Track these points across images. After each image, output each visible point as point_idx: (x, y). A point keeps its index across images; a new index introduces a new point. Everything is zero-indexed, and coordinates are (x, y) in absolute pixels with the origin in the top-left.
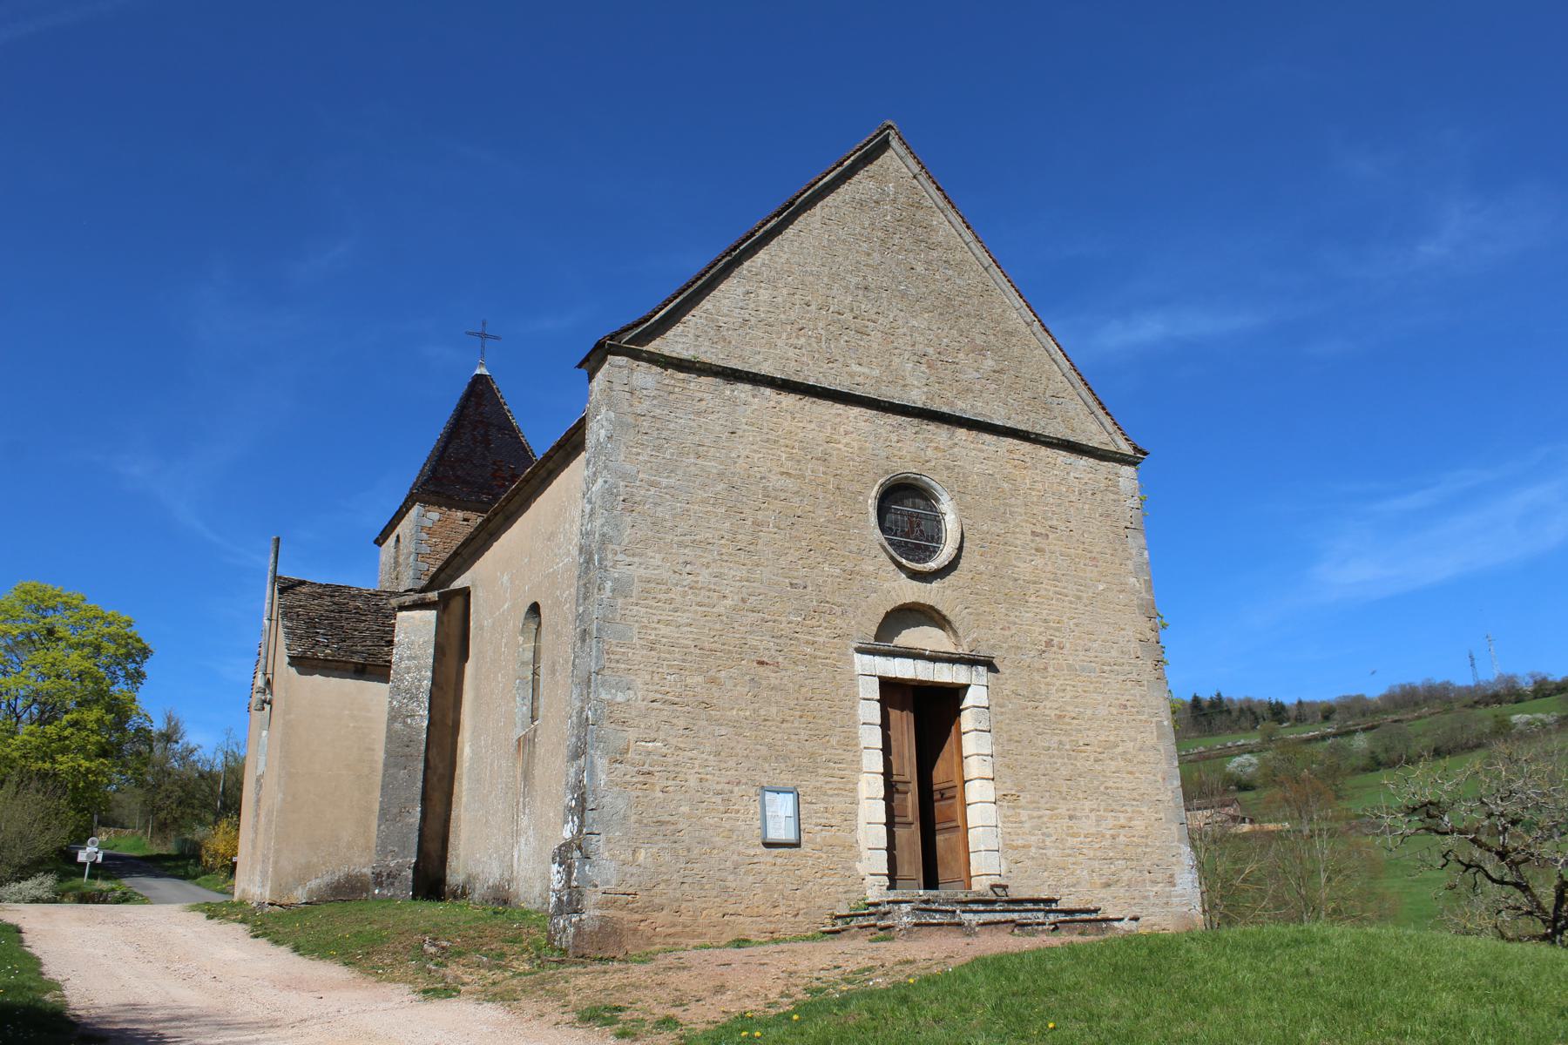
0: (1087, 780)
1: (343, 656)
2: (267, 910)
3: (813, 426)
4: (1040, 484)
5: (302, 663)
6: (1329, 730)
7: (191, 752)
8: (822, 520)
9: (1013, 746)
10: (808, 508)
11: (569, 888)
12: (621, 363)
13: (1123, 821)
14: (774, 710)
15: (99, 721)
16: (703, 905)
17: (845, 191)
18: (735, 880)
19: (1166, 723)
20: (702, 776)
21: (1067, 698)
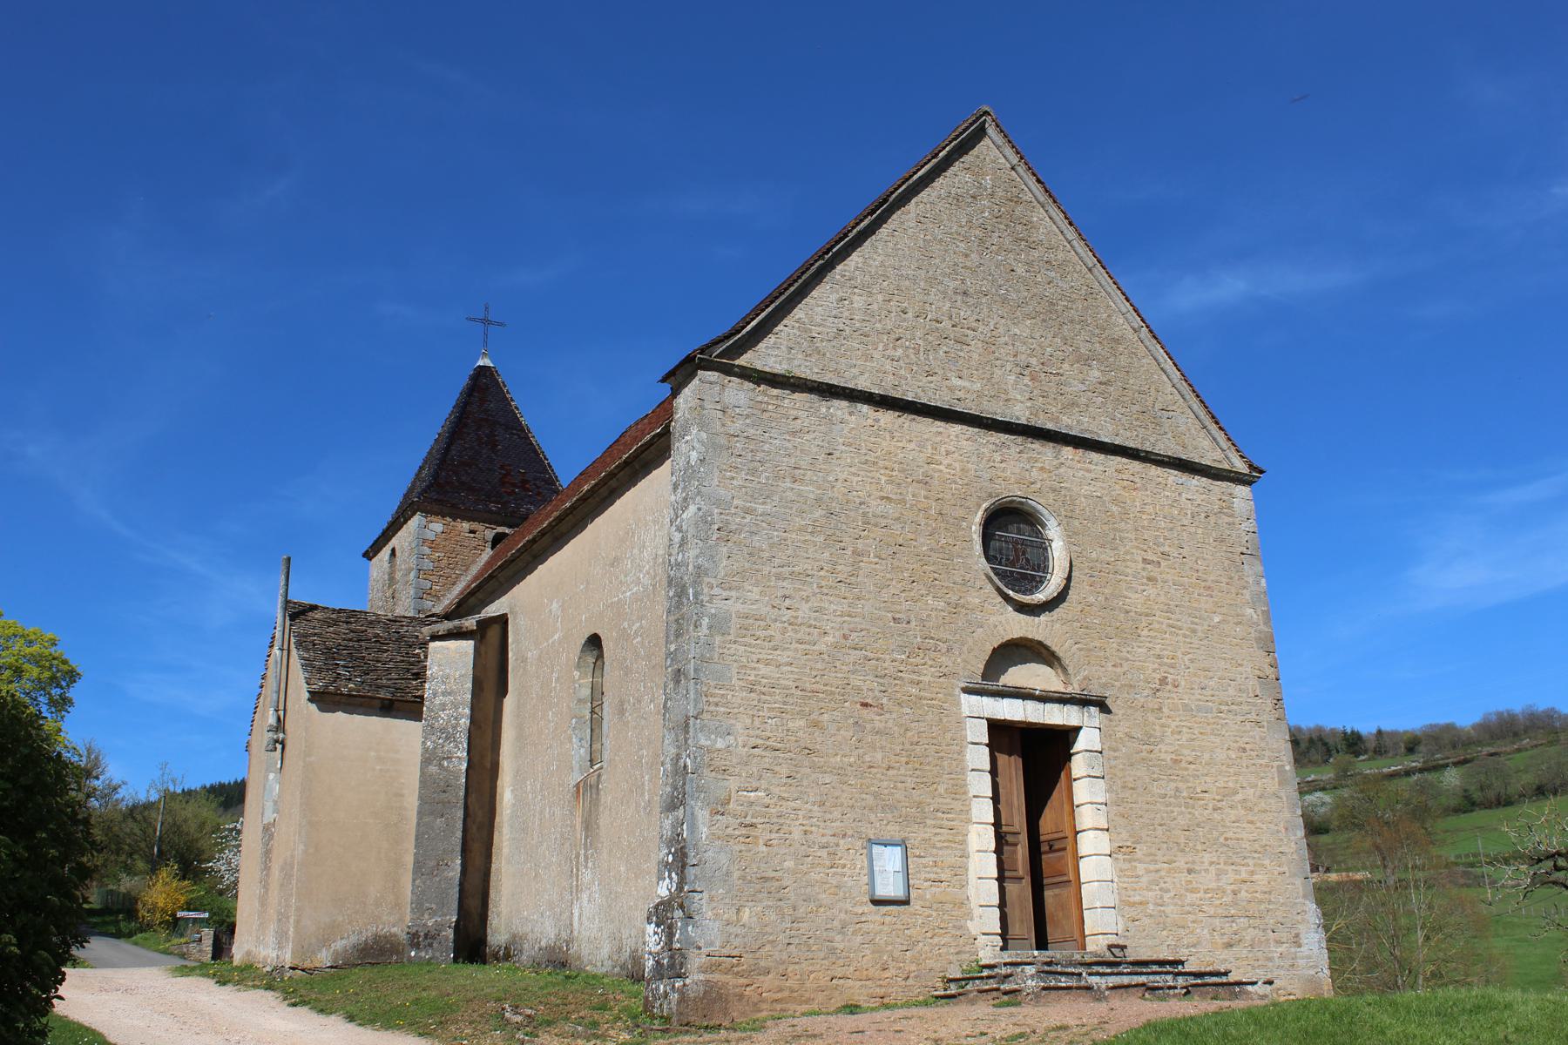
0: (1205, 830)
1: (369, 691)
2: (288, 975)
3: (912, 446)
4: (1151, 507)
5: (325, 699)
6: (1414, 764)
7: (115, 789)
8: (924, 549)
9: (1127, 794)
11: (670, 950)
12: (712, 379)
13: (1244, 875)
14: (879, 755)
16: (810, 968)
18: (843, 941)
19: (1288, 768)
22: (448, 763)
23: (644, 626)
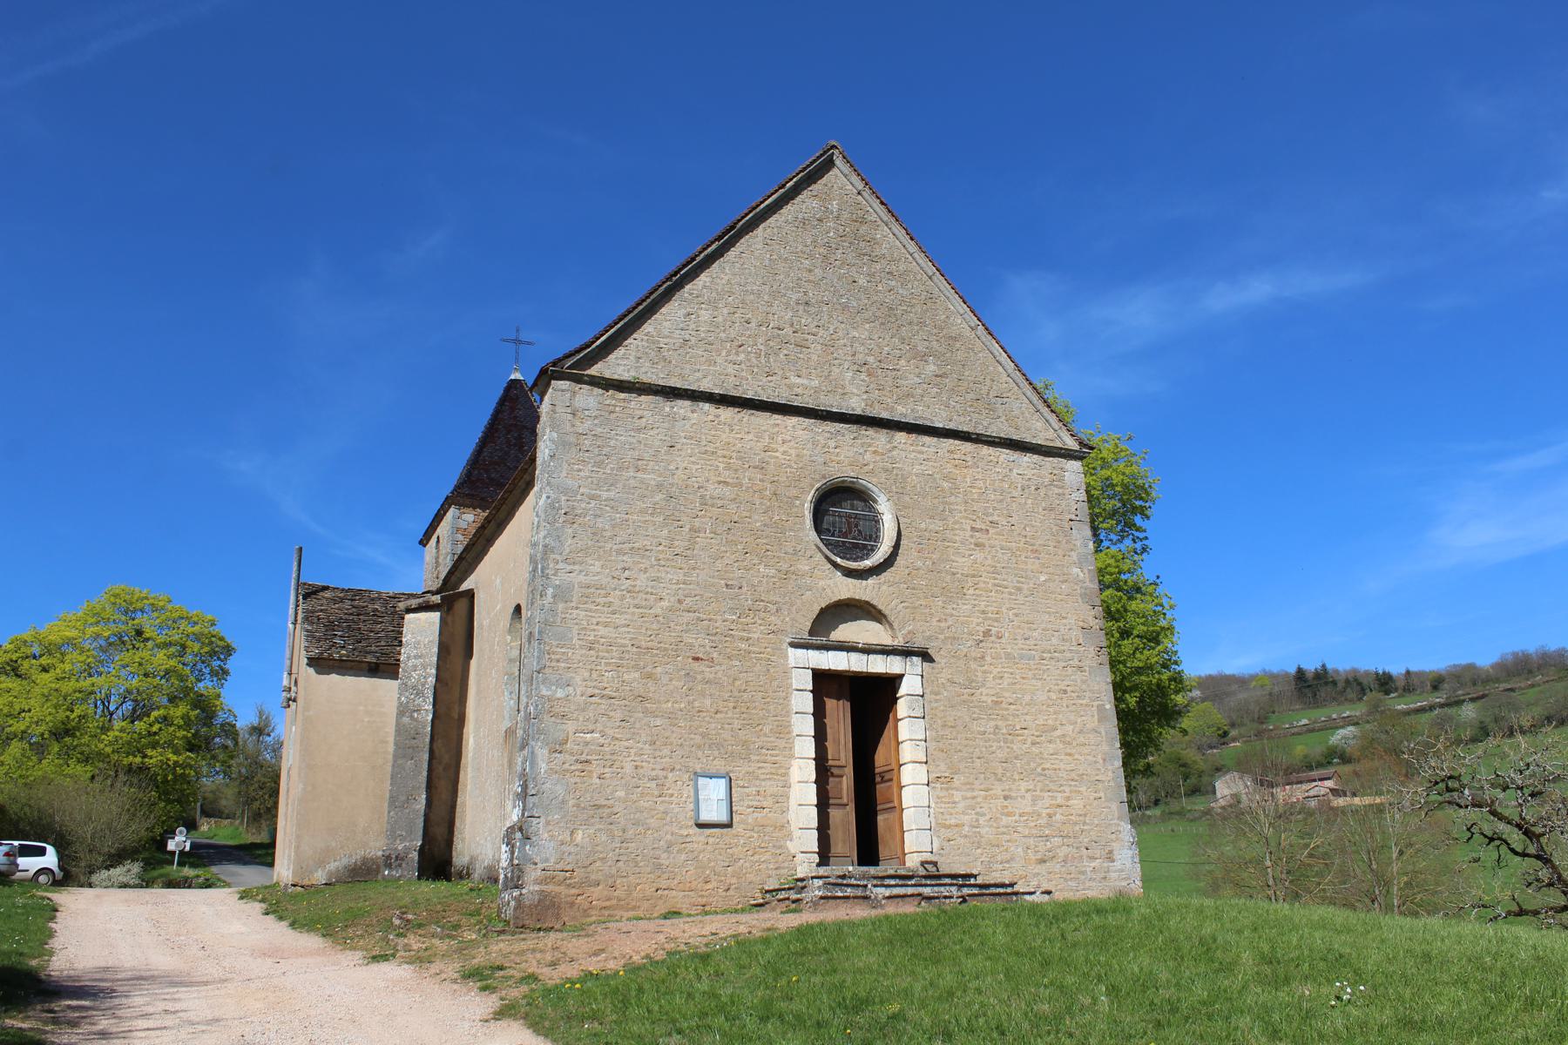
2: (290, 890)
3: (751, 436)
5: (319, 664)
6: (1438, 700)
10: (745, 514)
13: (1059, 801)
15: (185, 717)
17: (788, 211)
18: (668, 858)
19: (1108, 707)
20: (637, 763)
21: (1005, 685)
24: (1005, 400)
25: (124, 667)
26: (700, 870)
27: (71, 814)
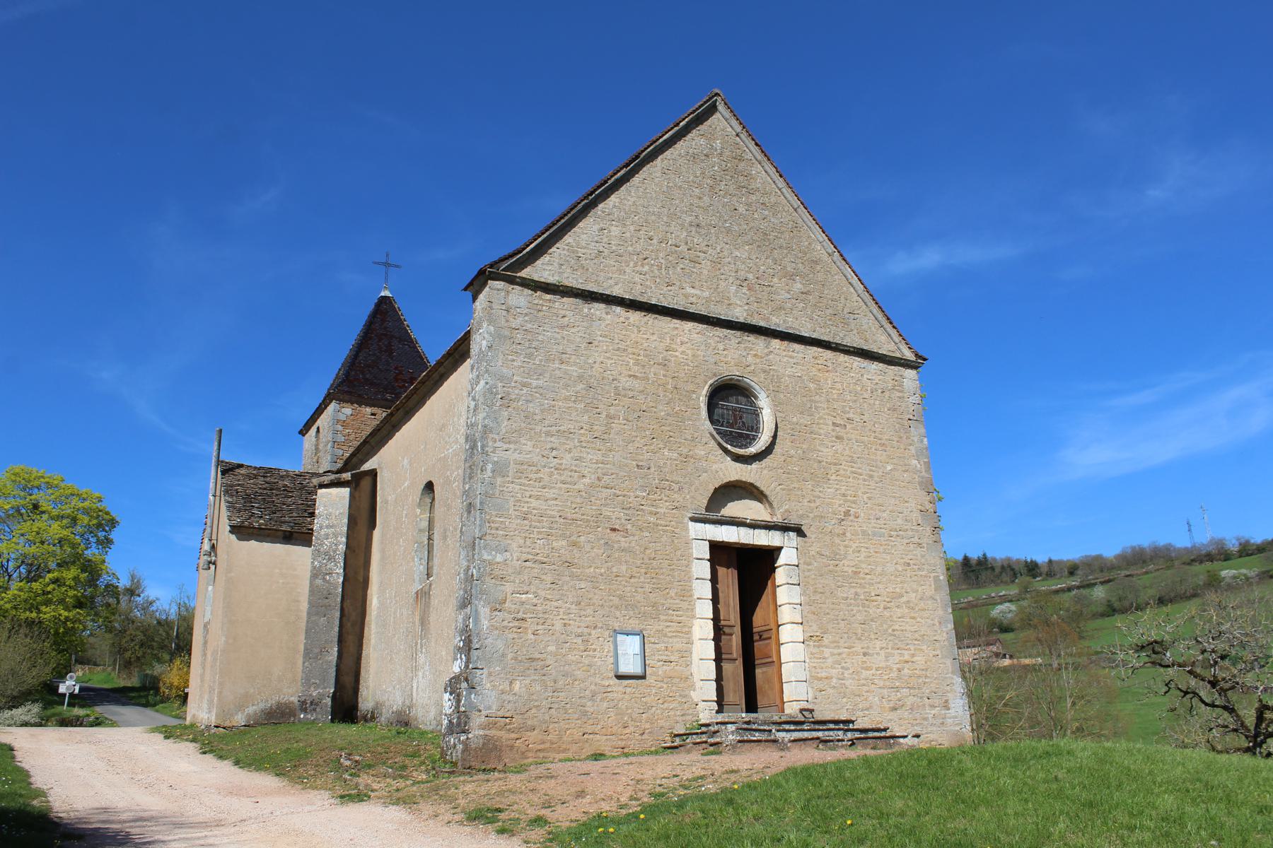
1: (274, 525)
2: (213, 731)
3: (655, 337)
5: (241, 531)
6: (1074, 583)
7: (151, 603)
8: (663, 414)
10: (651, 404)
11: (458, 712)
12: (499, 287)
13: (907, 657)
15: (76, 579)
17: (681, 146)
18: (593, 706)
19: (941, 578)
21: (862, 558)
22: (330, 577)
23: (460, 474)
24: (856, 316)
25: (22, 535)
26: (619, 717)
27: (975, 654)
